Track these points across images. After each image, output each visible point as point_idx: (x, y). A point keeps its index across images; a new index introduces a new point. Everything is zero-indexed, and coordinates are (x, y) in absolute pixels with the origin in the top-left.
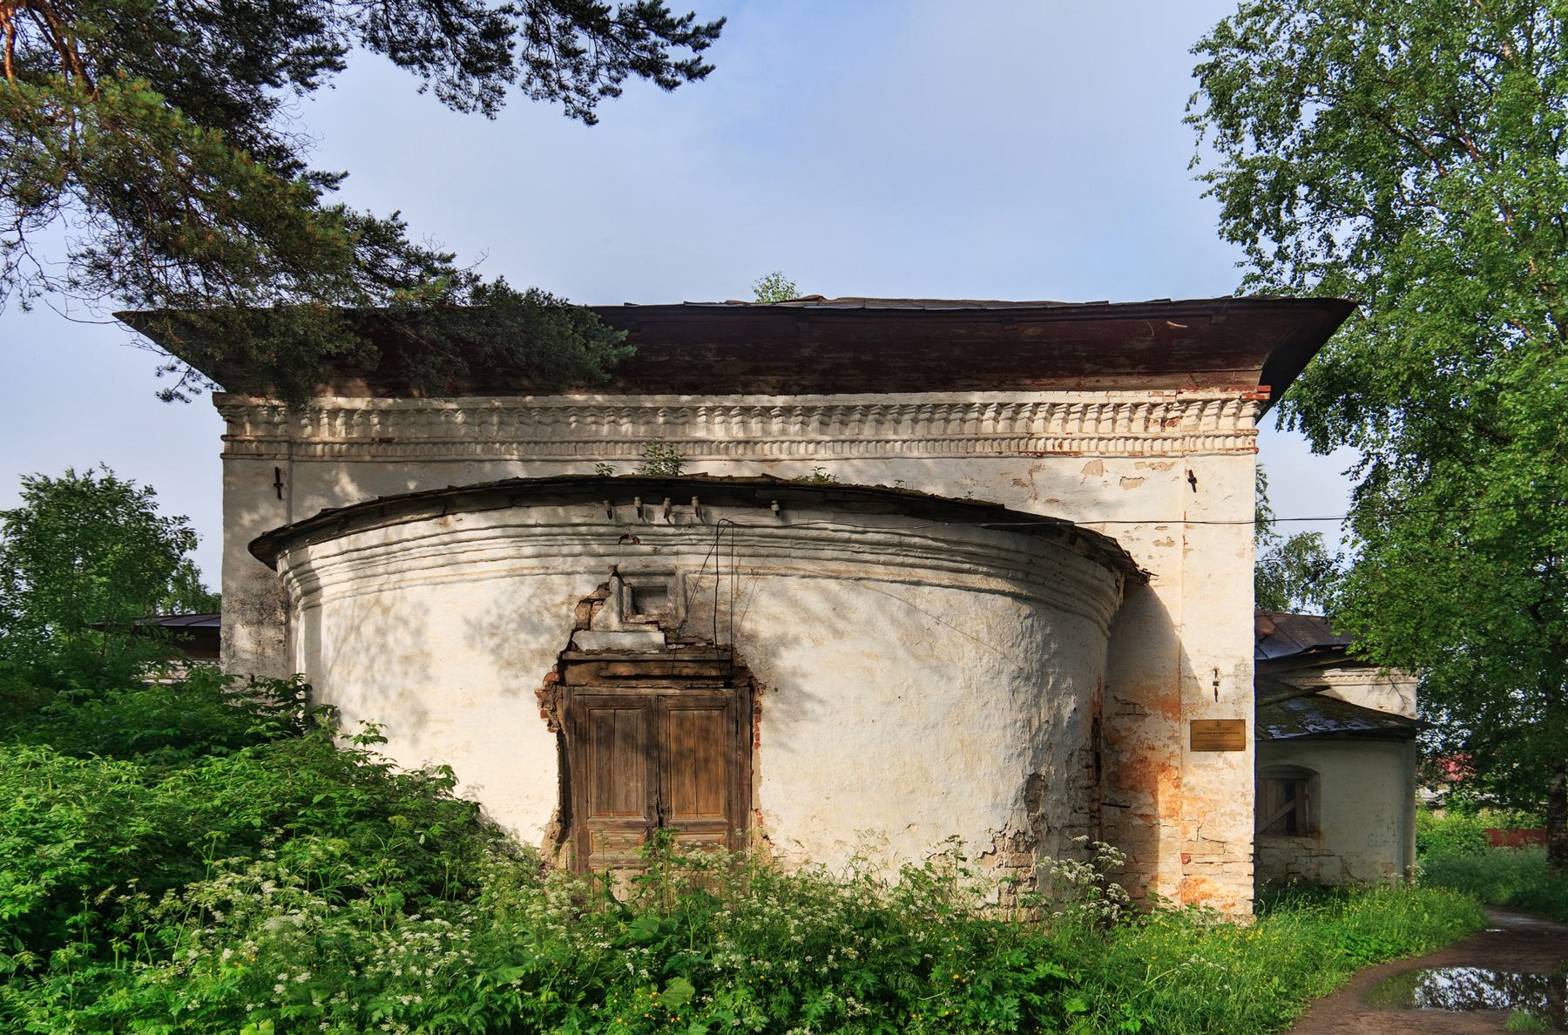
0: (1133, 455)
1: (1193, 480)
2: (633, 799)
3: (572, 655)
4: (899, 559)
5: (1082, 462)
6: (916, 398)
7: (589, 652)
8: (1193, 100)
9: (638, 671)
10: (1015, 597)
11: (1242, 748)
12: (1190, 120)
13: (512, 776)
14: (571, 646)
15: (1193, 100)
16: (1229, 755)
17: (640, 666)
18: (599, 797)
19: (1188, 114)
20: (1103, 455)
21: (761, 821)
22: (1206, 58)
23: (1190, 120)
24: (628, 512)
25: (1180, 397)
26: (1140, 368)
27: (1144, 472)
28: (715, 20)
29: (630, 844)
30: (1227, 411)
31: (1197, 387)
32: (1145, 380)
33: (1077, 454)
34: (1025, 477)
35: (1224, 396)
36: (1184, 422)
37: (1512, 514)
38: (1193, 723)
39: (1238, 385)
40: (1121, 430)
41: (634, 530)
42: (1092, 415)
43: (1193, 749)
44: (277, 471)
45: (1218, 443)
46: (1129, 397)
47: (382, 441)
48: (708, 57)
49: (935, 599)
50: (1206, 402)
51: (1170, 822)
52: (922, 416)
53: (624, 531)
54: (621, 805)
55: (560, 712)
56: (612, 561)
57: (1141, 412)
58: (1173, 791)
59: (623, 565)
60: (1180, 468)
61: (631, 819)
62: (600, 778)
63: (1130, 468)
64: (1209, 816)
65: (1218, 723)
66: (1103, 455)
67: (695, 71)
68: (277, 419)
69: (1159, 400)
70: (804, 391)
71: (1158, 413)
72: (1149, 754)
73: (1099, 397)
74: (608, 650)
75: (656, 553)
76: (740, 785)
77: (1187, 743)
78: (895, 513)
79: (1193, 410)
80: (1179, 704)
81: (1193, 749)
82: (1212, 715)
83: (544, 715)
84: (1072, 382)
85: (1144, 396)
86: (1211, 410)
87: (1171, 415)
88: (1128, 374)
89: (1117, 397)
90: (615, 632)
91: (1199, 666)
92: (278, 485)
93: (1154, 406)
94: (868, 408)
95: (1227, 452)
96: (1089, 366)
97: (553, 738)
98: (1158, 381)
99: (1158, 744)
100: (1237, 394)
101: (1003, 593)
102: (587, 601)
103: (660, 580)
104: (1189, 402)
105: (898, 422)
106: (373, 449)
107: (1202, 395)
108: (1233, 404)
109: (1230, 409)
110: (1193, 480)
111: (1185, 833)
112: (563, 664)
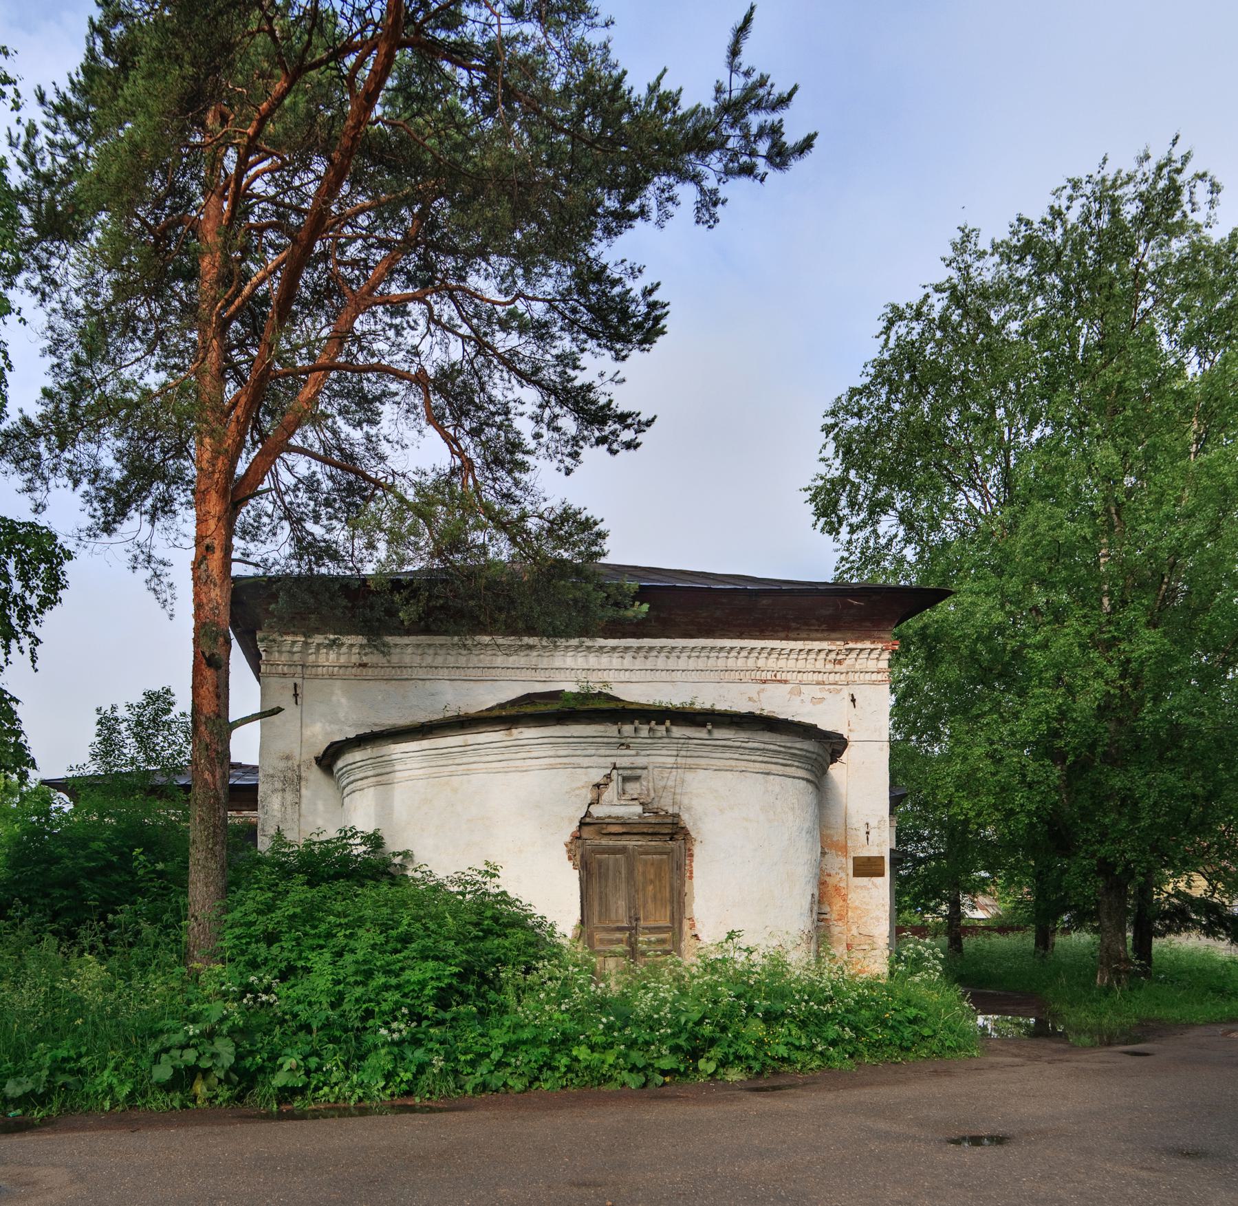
0: (818, 683)
1: (853, 700)
2: (620, 911)
3: (588, 820)
4: (761, 759)
5: (788, 687)
6: (691, 642)
7: (598, 818)
8: (824, 446)
9: (624, 830)
10: (808, 780)
11: (882, 875)
12: (822, 460)
13: (549, 892)
14: (588, 814)
15: (824, 446)
16: (874, 879)
17: (628, 828)
18: (600, 912)
19: (821, 456)
20: (801, 683)
21: (693, 926)
22: (830, 421)
23: (822, 460)
24: (628, 729)
25: (847, 646)
26: (824, 627)
27: (825, 694)
28: (651, 417)
29: (620, 941)
30: (872, 656)
31: (856, 640)
32: (826, 634)
33: (786, 682)
34: (755, 696)
35: (872, 646)
36: (847, 662)
37: (1043, 727)
38: (854, 858)
39: (880, 639)
40: (810, 667)
41: (629, 740)
42: (793, 656)
43: (855, 875)
44: (295, 685)
45: (868, 676)
46: (816, 645)
47: (360, 665)
48: (641, 437)
49: (775, 783)
50: (862, 650)
51: (840, 923)
52: (693, 654)
53: (623, 741)
54: (613, 916)
55: (578, 857)
56: (612, 760)
57: (822, 655)
58: (841, 903)
59: (621, 762)
60: (846, 692)
61: (619, 924)
62: (601, 898)
63: (816, 691)
64: (864, 920)
65: (869, 858)
66: (801, 683)
67: (631, 445)
68: (295, 649)
69: (834, 648)
70: (624, 636)
71: (832, 656)
72: (827, 879)
73: (799, 645)
74: (609, 817)
75: (637, 755)
76: (679, 903)
77: (851, 872)
78: (763, 730)
79: (853, 655)
80: (846, 846)
81: (855, 875)
82: (865, 853)
83: (570, 859)
84: (783, 635)
85: (825, 645)
86: (864, 655)
87: (840, 657)
88: (817, 630)
89: (810, 645)
90: (613, 807)
91: (857, 822)
92: (296, 695)
93: (830, 651)
94: (640, 648)
95: (873, 683)
96: (794, 625)
97: (576, 874)
98: (833, 635)
99: (833, 872)
100: (880, 646)
101: (803, 779)
102: (598, 786)
103: (639, 772)
104: (852, 650)
105: (678, 657)
106: (354, 671)
107: (859, 646)
108: (877, 652)
109: (874, 655)
110: (853, 700)
111: (849, 930)
112: (582, 824)
